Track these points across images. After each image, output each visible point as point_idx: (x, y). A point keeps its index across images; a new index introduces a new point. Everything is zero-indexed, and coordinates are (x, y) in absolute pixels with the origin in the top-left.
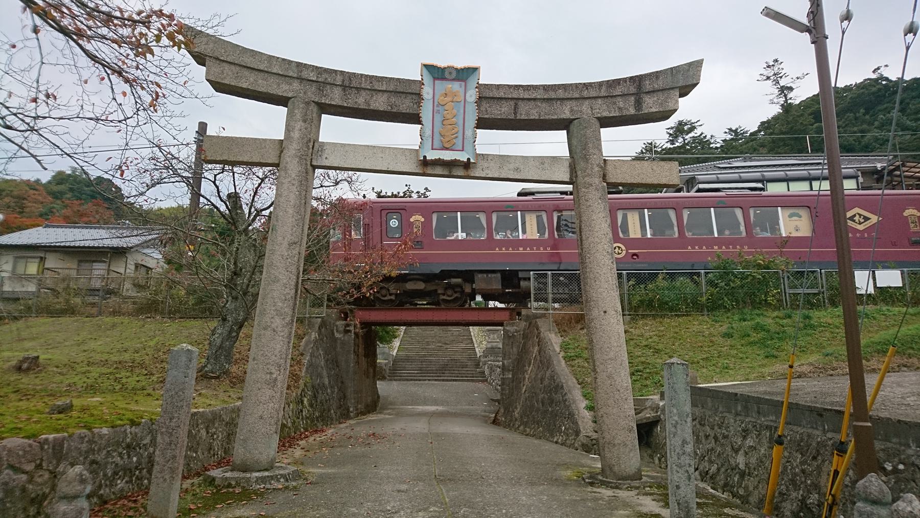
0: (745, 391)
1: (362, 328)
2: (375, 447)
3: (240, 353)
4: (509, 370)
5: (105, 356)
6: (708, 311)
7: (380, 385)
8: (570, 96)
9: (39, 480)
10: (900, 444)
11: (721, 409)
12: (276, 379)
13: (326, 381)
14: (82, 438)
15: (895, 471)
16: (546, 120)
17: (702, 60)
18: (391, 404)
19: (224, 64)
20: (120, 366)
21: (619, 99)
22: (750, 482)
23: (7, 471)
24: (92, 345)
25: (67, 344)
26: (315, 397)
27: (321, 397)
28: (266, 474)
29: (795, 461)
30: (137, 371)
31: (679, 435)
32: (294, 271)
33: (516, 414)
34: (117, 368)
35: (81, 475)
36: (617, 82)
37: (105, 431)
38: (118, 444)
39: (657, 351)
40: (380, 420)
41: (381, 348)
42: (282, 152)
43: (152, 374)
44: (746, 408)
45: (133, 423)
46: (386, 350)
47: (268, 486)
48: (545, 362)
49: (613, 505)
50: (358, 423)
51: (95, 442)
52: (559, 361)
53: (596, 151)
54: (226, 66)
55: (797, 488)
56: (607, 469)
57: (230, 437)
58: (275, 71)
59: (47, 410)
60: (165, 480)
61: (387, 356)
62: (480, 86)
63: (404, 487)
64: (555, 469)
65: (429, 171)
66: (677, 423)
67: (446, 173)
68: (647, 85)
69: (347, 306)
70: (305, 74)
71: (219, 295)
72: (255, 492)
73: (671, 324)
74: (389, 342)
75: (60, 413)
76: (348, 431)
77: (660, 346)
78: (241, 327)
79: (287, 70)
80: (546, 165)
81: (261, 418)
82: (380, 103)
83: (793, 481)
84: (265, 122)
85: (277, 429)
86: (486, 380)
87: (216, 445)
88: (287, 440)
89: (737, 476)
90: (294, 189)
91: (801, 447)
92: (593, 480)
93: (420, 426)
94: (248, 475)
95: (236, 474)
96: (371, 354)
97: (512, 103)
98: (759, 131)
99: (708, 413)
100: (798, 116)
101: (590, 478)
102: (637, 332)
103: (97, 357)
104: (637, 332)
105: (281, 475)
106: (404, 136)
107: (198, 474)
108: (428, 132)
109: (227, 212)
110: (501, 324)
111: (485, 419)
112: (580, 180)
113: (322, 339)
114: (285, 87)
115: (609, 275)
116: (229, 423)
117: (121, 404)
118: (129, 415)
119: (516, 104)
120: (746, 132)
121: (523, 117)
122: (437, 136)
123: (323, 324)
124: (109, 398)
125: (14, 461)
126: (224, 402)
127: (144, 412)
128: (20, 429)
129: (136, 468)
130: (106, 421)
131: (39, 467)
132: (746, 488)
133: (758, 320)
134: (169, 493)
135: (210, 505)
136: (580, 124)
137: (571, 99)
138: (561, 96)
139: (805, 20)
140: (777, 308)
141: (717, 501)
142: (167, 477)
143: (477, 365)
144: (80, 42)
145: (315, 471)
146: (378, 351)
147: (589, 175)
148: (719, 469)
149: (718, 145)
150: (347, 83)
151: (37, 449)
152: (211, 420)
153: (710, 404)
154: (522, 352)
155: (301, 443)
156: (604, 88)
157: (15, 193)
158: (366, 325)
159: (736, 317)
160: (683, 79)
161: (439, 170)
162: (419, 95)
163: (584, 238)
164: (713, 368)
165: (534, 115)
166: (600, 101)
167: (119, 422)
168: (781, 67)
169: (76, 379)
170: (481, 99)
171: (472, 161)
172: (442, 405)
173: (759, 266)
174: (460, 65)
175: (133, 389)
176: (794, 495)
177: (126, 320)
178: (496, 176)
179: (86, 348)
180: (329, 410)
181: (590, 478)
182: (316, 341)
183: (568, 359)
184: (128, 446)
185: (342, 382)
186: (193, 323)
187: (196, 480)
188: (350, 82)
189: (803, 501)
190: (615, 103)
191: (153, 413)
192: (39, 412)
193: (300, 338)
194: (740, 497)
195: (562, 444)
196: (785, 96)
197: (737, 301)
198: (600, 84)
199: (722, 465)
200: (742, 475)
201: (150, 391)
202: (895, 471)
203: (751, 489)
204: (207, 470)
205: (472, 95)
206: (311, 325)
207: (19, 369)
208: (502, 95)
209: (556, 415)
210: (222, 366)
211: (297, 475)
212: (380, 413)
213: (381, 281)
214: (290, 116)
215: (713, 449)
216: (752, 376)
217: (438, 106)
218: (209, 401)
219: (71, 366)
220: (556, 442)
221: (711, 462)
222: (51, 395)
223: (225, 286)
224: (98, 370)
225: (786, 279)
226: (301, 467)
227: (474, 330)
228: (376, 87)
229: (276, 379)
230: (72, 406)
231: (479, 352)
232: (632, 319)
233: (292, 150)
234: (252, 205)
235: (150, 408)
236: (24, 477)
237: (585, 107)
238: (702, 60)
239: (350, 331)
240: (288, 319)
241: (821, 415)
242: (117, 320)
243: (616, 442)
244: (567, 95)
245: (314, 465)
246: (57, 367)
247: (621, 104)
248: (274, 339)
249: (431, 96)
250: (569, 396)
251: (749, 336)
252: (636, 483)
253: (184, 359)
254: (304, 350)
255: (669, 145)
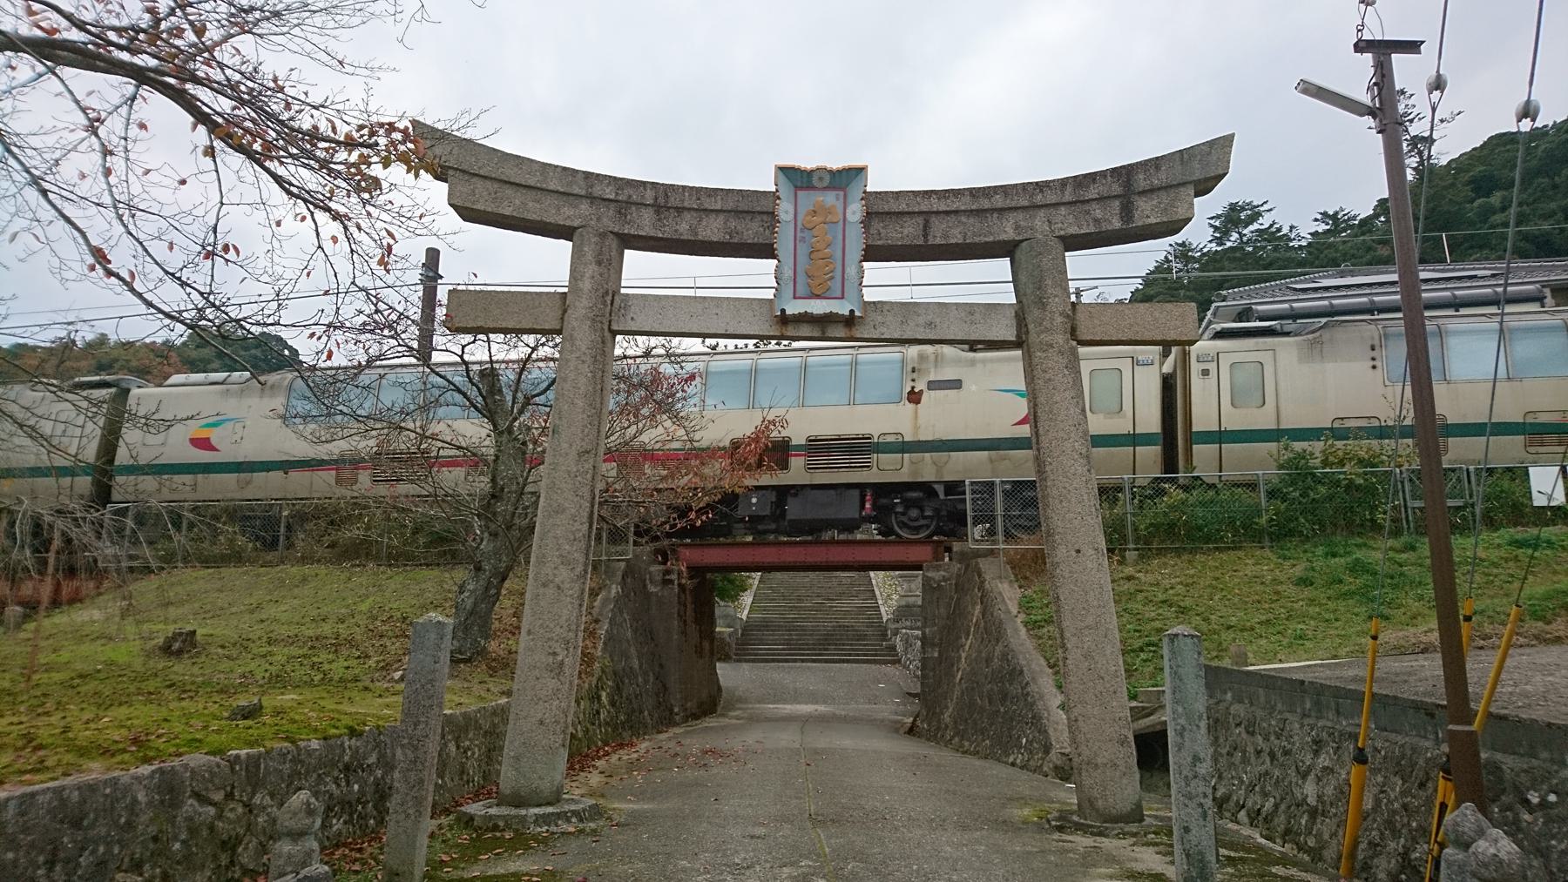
0: (1323, 677)
1: (691, 578)
2: (715, 771)
3: (500, 620)
4: (933, 645)
5: (293, 630)
6: (1272, 540)
7: (721, 668)
8: (1013, 204)
9: (231, 815)
10: (1552, 761)
11: (1279, 706)
12: (562, 663)
13: (636, 664)
14: (283, 755)
15: (1544, 804)
16: (975, 244)
17: (1233, 135)
18: (740, 700)
19: (474, 180)
20: (317, 644)
21: (1094, 205)
22: (1325, 827)
23: (190, 801)
24: (272, 611)
25: (234, 610)
26: (618, 688)
27: (628, 690)
28: (550, 810)
29: (1393, 790)
30: (345, 652)
31: (1189, 748)
32: (587, 495)
33: (947, 717)
34: (312, 648)
35: (308, 804)
36: (1091, 178)
37: (315, 744)
38: (334, 764)
39: (1183, 611)
40: (723, 728)
41: (721, 608)
42: (565, 311)
43: (368, 657)
44: (1317, 704)
45: (353, 733)
46: (731, 611)
47: (553, 829)
48: (993, 631)
49: (1089, 860)
50: (687, 732)
51: (301, 761)
52: (1016, 630)
53: (1058, 291)
54: (479, 183)
55: (1396, 834)
56: (1086, 804)
57: (492, 753)
58: (552, 187)
59: (226, 714)
60: (408, 816)
61: (731, 621)
62: (867, 196)
63: (760, 831)
64: (1004, 806)
65: (790, 331)
66: (1184, 728)
67: (816, 334)
68: (1141, 182)
69: (666, 542)
70: (597, 191)
71: (469, 527)
72: (535, 838)
73: (1206, 566)
74: (735, 598)
75: (245, 718)
76: (672, 744)
77: (1188, 602)
78: (504, 580)
79: (570, 184)
80: (977, 316)
81: (541, 723)
82: (712, 229)
83: (1389, 823)
84: (541, 263)
85: (564, 740)
86: (899, 661)
87: (472, 767)
88: (579, 759)
89: (1306, 817)
90: (585, 369)
91: (1402, 766)
92: (1064, 824)
93: (786, 738)
94: (523, 812)
95: (505, 811)
96: (704, 616)
97: (920, 220)
98: (1376, 216)
99: (1259, 713)
100: (1445, 188)
101: (1056, 819)
102: (1150, 578)
103: (283, 631)
104: (1150, 578)
105: (574, 812)
106: (751, 278)
107: (447, 812)
108: (788, 273)
109: (480, 399)
110: (918, 567)
111: (895, 728)
112: (1033, 338)
113: (627, 596)
114: (567, 211)
115: (1084, 491)
116: (488, 732)
117: (329, 704)
118: (346, 721)
119: (927, 222)
120: (1354, 218)
121: (938, 241)
122: (801, 279)
123: (630, 571)
124: (308, 694)
125: (198, 786)
126: (481, 698)
127: (365, 715)
128: (200, 741)
129: (358, 801)
130: (316, 730)
131: (229, 796)
132: (1319, 836)
133: (1359, 554)
134: (416, 835)
135: (471, 853)
136: (1032, 248)
137: (1016, 209)
138: (1000, 205)
139: (1366, 99)
140: (1396, 533)
141: (1269, 859)
142: (411, 811)
143: (884, 636)
144: (267, 164)
145: (622, 807)
146: (717, 612)
147: (1047, 330)
148: (1276, 806)
149: (1304, 243)
150: (661, 201)
151: (227, 770)
152: (458, 728)
153: (1262, 699)
154: (948, 616)
155: (598, 763)
156: (1069, 189)
157: (134, 363)
158: (696, 571)
159: (1320, 551)
160: (1202, 166)
161: (805, 330)
162: (772, 214)
163: (1041, 431)
164: (1279, 637)
165: (956, 237)
166: (1063, 210)
167: (334, 731)
168: (1411, 102)
169: (253, 666)
170: (870, 216)
171: (857, 313)
172: (825, 702)
173: (1361, 462)
174: (835, 164)
175: (341, 680)
176: (1393, 845)
177: (322, 570)
178: (896, 336)
179: (264, 617)
180: (641, 712)
181: (1056, 819)
182: (617, 600)
183: (1032, 626)
184: (347, 768)
185: (661, 666)
186: (425, 573)
187: (444, 820)
188: (666, 199)
189: (1405, 855)
190: (1088, 212)
191: (379, 718)
192: (215, 717)
193: (594, 594)
194: (1309, 851)
195: (1022, 768)
196: (1420, 153)
197: (1323, 527)
198: (1064, 182)
199: (1282, 799)
200: (1313, 813)
201: (367, 683)
202: (1544, 804)
203: (1326, 836)
204: (458, 804)
205: (855, 212)
206: (610, 573)
207: (166, 649)
208: (903, 207)
209: (1012, 719)
210: (478, 642)
211: (596, 812)
212: (723, 715)
213: (719, 502)
214: (577, 256)
215: (1267, 773)
216: (1343, 651)
217: (802, 230)
218: (461, 697)
219: (244, 644)
220: (1013, 764)
221: (1265, 795)
222: (221, 692)
223: (478, 516)
224: (286, 650)
225: (1407, 484)
226: (601, 801)
227: (876, 577)
228: (707, 206)
229: (562, 663)
230: (261, 707)
231: (886, 612)
232: (1141, 557)
233: (580, 309)
234: (516, 391)
235: (379, 708)
236: (212, 811)
237: (1039, 221)
238: (1233, 135)
239: (671, 582)
240: (579, 569)
241: (1432, 716)
242: (307, 569)
243: (1099, 761)
244: (1009, 203)
245: (622, 797)
246: (223, 647)
247: (1098, 213)
248: (557, 602)
249: (790, 217)
250: (1032, 688)
251: (1341, 582)
252: (1133, 828)
253: (433, 636)
254: (600, 614)
255: (1214, 247)
